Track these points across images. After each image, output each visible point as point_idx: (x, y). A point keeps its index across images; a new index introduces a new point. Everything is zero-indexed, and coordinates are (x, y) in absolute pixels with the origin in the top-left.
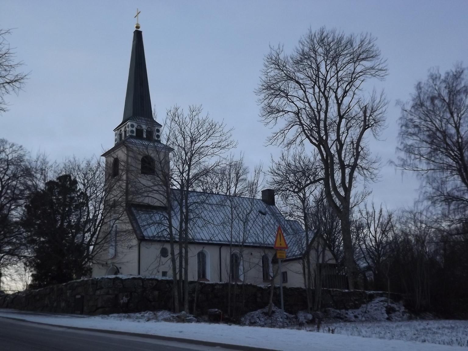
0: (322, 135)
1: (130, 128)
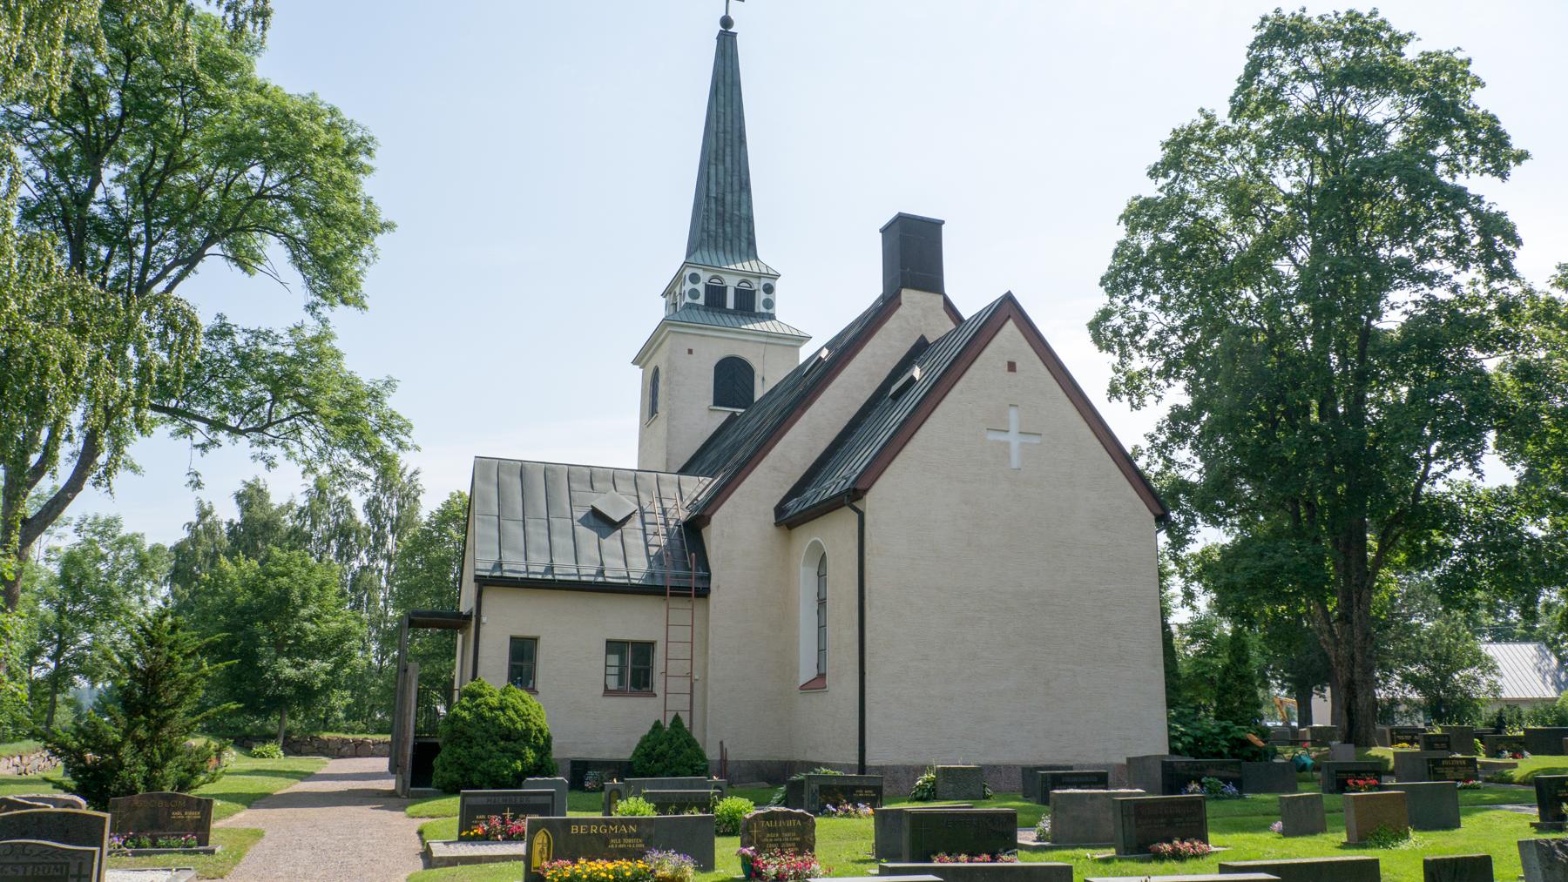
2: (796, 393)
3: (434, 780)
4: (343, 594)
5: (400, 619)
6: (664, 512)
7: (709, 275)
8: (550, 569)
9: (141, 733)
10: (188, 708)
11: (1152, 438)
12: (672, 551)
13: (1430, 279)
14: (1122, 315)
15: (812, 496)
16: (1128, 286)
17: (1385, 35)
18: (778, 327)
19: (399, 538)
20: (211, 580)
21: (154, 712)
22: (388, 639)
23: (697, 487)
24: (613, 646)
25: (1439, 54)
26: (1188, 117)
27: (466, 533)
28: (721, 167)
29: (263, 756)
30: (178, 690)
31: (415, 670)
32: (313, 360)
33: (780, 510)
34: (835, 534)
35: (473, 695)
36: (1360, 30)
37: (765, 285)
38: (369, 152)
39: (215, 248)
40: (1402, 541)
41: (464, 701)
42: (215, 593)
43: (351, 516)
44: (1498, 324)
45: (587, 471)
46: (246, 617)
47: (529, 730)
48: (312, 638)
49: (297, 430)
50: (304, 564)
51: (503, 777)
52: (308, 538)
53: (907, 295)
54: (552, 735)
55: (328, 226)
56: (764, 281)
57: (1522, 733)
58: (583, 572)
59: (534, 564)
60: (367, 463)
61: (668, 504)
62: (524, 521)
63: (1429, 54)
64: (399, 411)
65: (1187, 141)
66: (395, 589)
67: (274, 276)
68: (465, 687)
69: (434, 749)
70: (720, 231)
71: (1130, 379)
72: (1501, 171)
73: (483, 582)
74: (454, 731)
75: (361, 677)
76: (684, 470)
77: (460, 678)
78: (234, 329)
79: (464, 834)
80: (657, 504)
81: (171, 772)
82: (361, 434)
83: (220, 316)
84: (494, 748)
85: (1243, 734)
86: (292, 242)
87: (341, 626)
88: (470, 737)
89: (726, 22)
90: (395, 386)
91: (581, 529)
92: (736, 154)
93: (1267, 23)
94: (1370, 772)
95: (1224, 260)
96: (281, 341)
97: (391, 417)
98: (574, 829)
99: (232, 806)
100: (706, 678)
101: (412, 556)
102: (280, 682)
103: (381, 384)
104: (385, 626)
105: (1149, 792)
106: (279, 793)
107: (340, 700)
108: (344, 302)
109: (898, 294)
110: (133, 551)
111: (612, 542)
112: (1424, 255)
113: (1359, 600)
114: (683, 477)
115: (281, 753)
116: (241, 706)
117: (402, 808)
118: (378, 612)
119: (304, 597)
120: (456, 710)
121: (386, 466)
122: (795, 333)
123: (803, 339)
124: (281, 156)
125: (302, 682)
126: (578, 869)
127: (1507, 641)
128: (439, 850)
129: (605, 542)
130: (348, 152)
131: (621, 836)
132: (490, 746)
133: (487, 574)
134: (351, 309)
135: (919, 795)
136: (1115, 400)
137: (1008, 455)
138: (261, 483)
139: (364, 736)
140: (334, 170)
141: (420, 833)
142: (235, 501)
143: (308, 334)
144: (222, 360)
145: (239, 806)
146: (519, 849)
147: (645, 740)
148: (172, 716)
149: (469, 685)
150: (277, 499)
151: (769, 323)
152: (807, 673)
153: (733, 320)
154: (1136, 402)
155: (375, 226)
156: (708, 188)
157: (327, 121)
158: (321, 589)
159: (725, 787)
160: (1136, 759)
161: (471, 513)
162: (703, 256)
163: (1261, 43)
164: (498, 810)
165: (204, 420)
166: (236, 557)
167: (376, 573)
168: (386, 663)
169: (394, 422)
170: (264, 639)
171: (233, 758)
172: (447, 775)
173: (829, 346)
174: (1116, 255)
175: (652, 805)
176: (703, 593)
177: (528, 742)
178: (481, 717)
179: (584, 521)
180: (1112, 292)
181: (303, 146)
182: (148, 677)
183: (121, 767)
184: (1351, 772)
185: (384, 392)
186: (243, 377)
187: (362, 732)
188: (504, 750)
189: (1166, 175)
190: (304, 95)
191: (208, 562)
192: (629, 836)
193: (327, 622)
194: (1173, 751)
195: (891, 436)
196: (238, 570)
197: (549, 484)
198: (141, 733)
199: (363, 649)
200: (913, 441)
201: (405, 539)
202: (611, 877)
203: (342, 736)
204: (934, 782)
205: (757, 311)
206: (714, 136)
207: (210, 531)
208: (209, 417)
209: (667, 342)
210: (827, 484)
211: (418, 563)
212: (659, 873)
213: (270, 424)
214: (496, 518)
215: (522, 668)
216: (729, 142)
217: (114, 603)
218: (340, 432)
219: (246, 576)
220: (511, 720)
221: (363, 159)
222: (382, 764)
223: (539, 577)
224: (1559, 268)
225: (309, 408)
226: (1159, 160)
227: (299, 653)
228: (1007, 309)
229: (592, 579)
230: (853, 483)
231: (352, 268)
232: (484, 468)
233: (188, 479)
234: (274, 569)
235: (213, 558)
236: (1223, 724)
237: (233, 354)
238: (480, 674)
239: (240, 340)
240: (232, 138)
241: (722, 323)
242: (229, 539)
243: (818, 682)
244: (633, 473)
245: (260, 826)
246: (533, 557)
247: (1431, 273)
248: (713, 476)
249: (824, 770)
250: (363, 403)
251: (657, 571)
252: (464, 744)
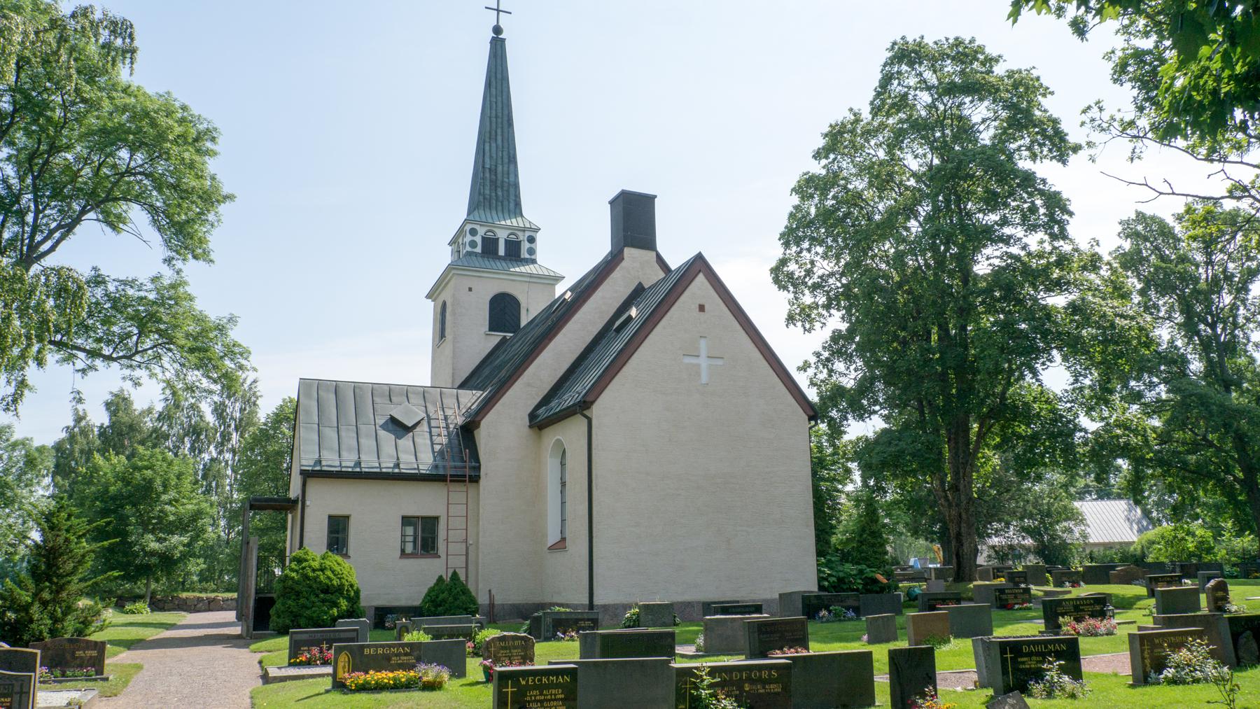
2: (546, 326)
3: (271, 625)
4: (196, 482)
5: (242, 501)
6: (446, 418)
8: (358, 464)
9: (46, 595)
10: (81, 576)
11: (818, 355)
12: (451, 448)
13: (1006, 240)
14: (797, 262)
15: (556, 406)
16: (798, 242)
17: (981, 57)
18: (538, 269)
19: (242, 436)
20: (86, 473)
21: (55, 580)
22: (233, 517)
23: (471, 398)
24: (407, 520)
25: (1020, 72)
26: (841, 115)
27: (294, 431)
28: (494, 145)
29: (134, 613)
30: (73, 562)
31: (255, 542)
32: (170, 302)
33: (532, 416)
34: (571, 434)
35: (299, 561)
37: (529, 237)
38: (213, 139)
39: (92, 215)
40: (996, 429)
41: (293, 565)
42: (90, 483)
43: (201, 417)
44: (1056, 274)
45: (387, 388)
46: (118, 503)
47: (342, 585)
48: (171, 518)
49: (158, 357)
50: (164, 459)
51: (323, 620)
52: (167, 437)
53: (628, 251)
54: (360, 588)
55: (182, 198)
56: (528, 234)
57: (1081, 569)
58: (383, 465)
59: (346, 461)
60: (215, 382)
61: (449, 412)
62: (338, 427)
63: (1012, 71)
64: (240, 341)
65: (841, 133)
66: (239, 476)
67: (139, 236)
68: (294, 554)
69: (271, 602)
70: (494, 194)
71: (803, 310)
72: (1062, 159)
73: (307, 475)
74: (285, 588)
75: (212, 548)
76: (462, 386)
77: (291, 551)
78: (107, 279)
79: (292, 661)
80: (440, 413)
81: (70, 624)
82: (210, 359)
83: (95, 269)
84: (316, 600)
85: (873, 574)
86: (152, 210)
87: (196, 508)
88: (297, 592)
89: (497, 30)
90: (237, 322)
91: (382, 433)
92: (506, 135)
93: (896, 47)
94: (953, 599)
95: (870, 219)
96: (145, 288)
97: (234, 345)
98: (366, 651)
99: (116, 648)
100: (478, 542)
101: (252, 450)
102: (146, 554)
103: (225, 321)
104: (231, 507)
105: (772, 615)
106: (151, 638)
107: (196, 566)
108: (195, 257)
109: (621, 252)
110: (23, 452)
111: (405, 442)
112: (1004, 222)
113: (964, 474)
114: (460, 391)
115: (149, 610)
116: (122, 573)
117: (247, 646)
118: (225, 495)
119: (165, 486)
120: (287, 571)
121: (229, 383)
122: (552, 274)
123: (558, 279)
124: (142, 144)
125: (164, 553)
126: (368, 677)
127: (1109, 498)
128: (273, 672)
129: (400, 442)
130: (196, 140)
131: (398, 655)
132: (313, 598)
133: (310, 468)
134: (201, 262)
135: (627, 624)
136: (792, 326)
137: (698, 374)
138: (126, 393)
139: (216, 594)
140: (186, 155)
141: (260, 662)
142: (104, 408)
143: (166, 282)
144: (97, 303)
145: (122, 649)
146: (329, 670)
147: (431, 590)
148: (69, 582)
149: (297, 553)
150: (139, 405)
151: (532, 266)
152: (553, 537)
153: (504, 264)
154: (807, 326)
155: (219, 198)
157: (179, 115)
158: (178, 479)
159: (484, 623)
160: (784, 594)
161: (297, 422)
162: (480, 214)
163: (890, 62)
164: (317, 643)
165: (84, 350)
166: (107, 454)
167: (223, 464)
168: (232, 535)
169: (236, 350)
170: (133, 520)
171: (110, 614)
172: (280, 621)
173: (571, 289)
174: (792, 216)
175: (430, 636)
176: (475, 479)
177: (342, 594)
178: (306, 577)
179: (384, 427)
180: (787, 245)
181: (161, 137)
182: (50, 553)
183: (31, 621)
184: (938, 599)
185: (228, 326)
186: (115, 317)
187: (213, 591)
188: (323, 601)
189: (827, 157)
190: (161, 93)
191: (84, 458)
192: (406, 654)
193: (183, 504)
194: (821, 588)
195: (612, 361)
196: (110, 465)
197: (358, 398)
198: (46, 595)
199: (213, 525)
200: (628, 365)
201: (246, 436)
202: (391, 682)
203: (198, 595)
204: (638, 615)
205: (522, 257)
206: (488, 119)
207: (84, 432)
208: (88, 348)
209: (452, 283)
210: (565, 397)
211: (257, 455)
212: (425, 679)
213: (137, 352)
214: (316, 426)
215: (338, 538)
217: (9, 494)
218: (192, 357)
219: (117, 470)
220: (329, 578)
221: (209, 145)
222: (231, 616)
223: (350, 470)
224: (1120, 223)
225: (168, 339)
226: (821, 147)
227: (161, 530)
228: (699, 265)
229: (390, 470)
230: (583, 397)
231: (200, 229)
232: (305, 384)
233: (72, 396)
234: (140, 464)
235: (88, 454)
236: (860, 567)
237: (106, 298)
238: (305, 545)
239: (111, 287)
240: (104, 131)
241: (495, 267)
242: (99, 439)
243: (561, 545)
244: (422, 389)
245: (139, 661)
246: (345, 454)
247: (1007, 236)
248: (484, 390)
249: (558, 608)
250: (211, 335)
251: (440, 463)
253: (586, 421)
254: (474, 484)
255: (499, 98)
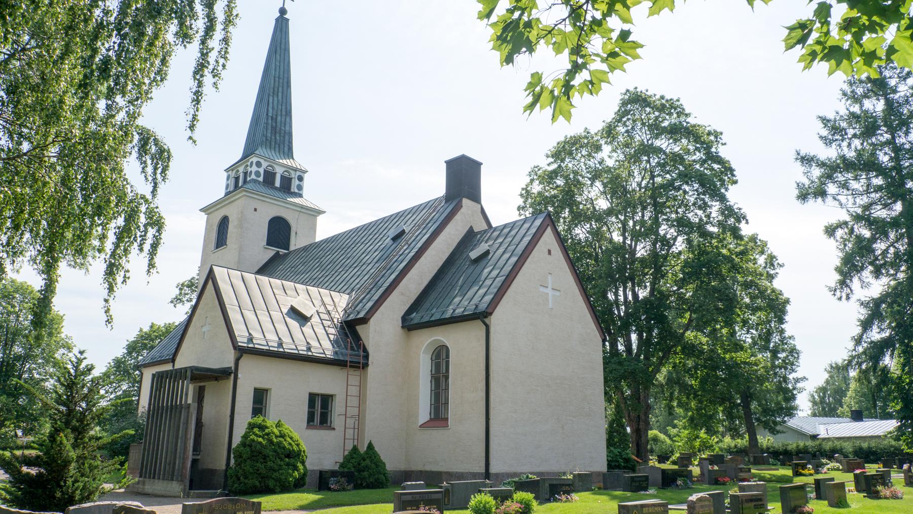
0: (640, 214)
1: (254, 168)
7: (268, 164)
28: (276, 99)
33: (404, 319)
36: (668, 106)
37: (299, 176)
56: (298, 173)
58: (299, 348)
70: (273, 137)
89: (283, 11)
92: (285, 93)
156: (268, 110)
163: (624, 103)
176: (366, 365)
205: (292, 190)
216: (281, 85)
252: (262, 460)
253: (484, 327)
254: (358, 373)
255: (282, 64)
